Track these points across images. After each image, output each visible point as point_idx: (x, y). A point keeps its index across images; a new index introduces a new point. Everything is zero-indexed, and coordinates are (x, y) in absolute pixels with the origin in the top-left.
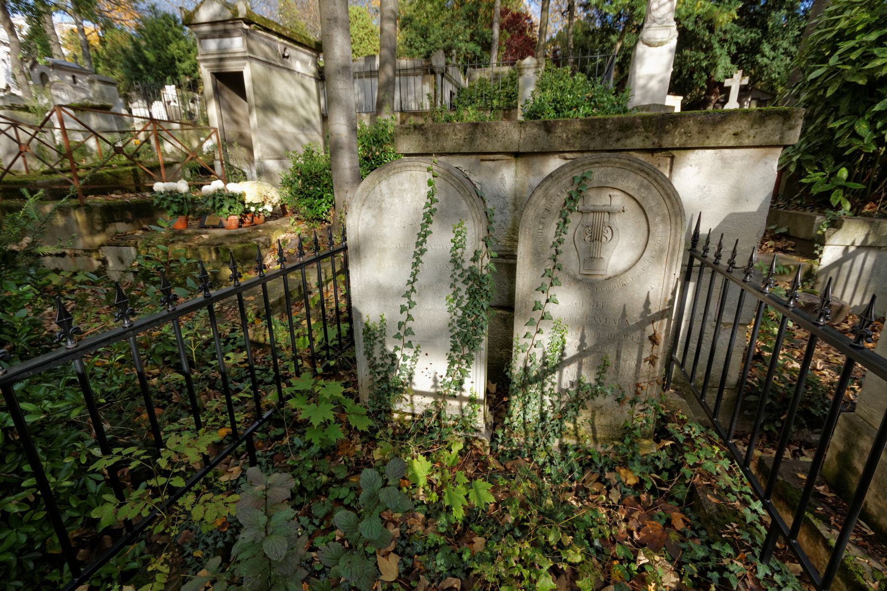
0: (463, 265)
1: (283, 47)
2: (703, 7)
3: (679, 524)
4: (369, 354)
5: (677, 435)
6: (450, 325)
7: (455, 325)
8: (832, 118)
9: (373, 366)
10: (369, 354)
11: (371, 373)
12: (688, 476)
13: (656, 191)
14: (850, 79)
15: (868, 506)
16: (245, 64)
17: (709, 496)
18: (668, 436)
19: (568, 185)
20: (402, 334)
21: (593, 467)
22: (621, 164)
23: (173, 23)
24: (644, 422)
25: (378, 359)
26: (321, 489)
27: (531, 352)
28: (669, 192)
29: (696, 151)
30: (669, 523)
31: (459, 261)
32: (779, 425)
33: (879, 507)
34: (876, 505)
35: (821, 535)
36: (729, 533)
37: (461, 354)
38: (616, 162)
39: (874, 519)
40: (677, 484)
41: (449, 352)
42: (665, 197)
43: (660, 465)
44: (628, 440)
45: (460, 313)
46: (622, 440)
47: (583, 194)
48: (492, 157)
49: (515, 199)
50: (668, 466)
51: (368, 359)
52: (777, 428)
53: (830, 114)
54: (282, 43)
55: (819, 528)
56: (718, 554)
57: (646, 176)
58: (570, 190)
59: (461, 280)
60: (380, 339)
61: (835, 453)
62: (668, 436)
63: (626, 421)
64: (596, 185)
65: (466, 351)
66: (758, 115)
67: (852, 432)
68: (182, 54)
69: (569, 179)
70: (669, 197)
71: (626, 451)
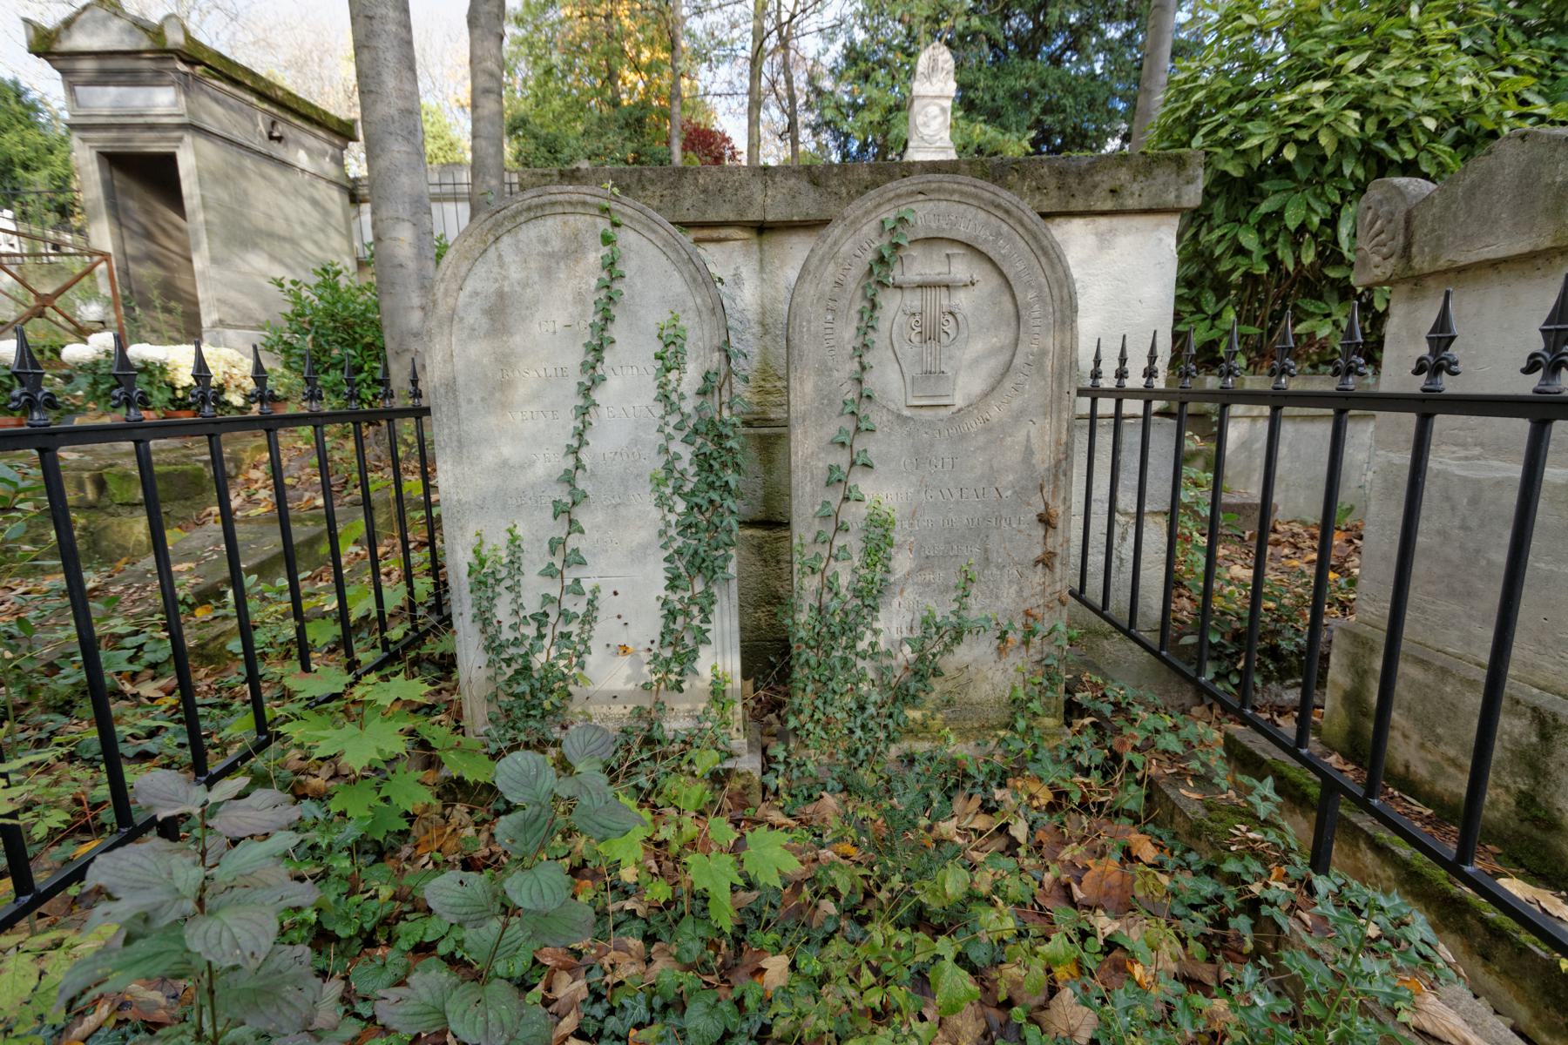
0: (683, 404)
1: (269, 120)
2: (985, 133)
3: (1148, 852)
4: (484, 619)
5: (1098, 705)
6: (662, 533)
7: (673, 532)
8: (1204, 230)
9: (493, 647)
10: (484, 619)
11: (490, 664)
12: (1138, 765)
13: (1022, 244)
14: (1222, 167)
15: (1412, 768)
16: (180, 139)
17: (1183, 791)
18: (1082, 711)
19: (873, 235)
20: (559, 566)
21: (968, 785)
22: (962, 193)
23: (12, 95)
24: (1046, 683)
25: (505, 627)
26: (374, 931)
27: (828, 573)
28: (1045, 243)
29: (1058, 220)
30: (1128, 856)
31: (674, 397)
32: (1236, 680)
33: (1431, 763)
34: (1424, 761)
35: (1361, 830)
36: (1240, 843)
37: (688, 595)
38: (953, 192)
39: (1427, 788)
40: (1124, 786)
41: (663, 594)
42: (1039, 253)
43: (1083, 759)
44: (1021, 724)
45: (681, 506)
46: (1011, 727)
47: (902, 253)
48: (715, 233)
49: (763, 314)
50: (1098, 759)
51: (483, 631)
52: (1234, 686)
53: (1201, 225)
54: (265, 111)
55: (1354, 820)
56: (1234, 879)
57: (1005, 216)
58: (877, 244)
59: (679, 436)
60: (508, 583)
61: (1339, 695)
62: (1082, 711)
63: (1014, 688)
64: (922, 235)
65: (699, 587)
66: (1141, 160)
67: (1360, 651)
68: (32, 154)
69: (875, 223)
70: (1045, 253)
71: (1021, 745)
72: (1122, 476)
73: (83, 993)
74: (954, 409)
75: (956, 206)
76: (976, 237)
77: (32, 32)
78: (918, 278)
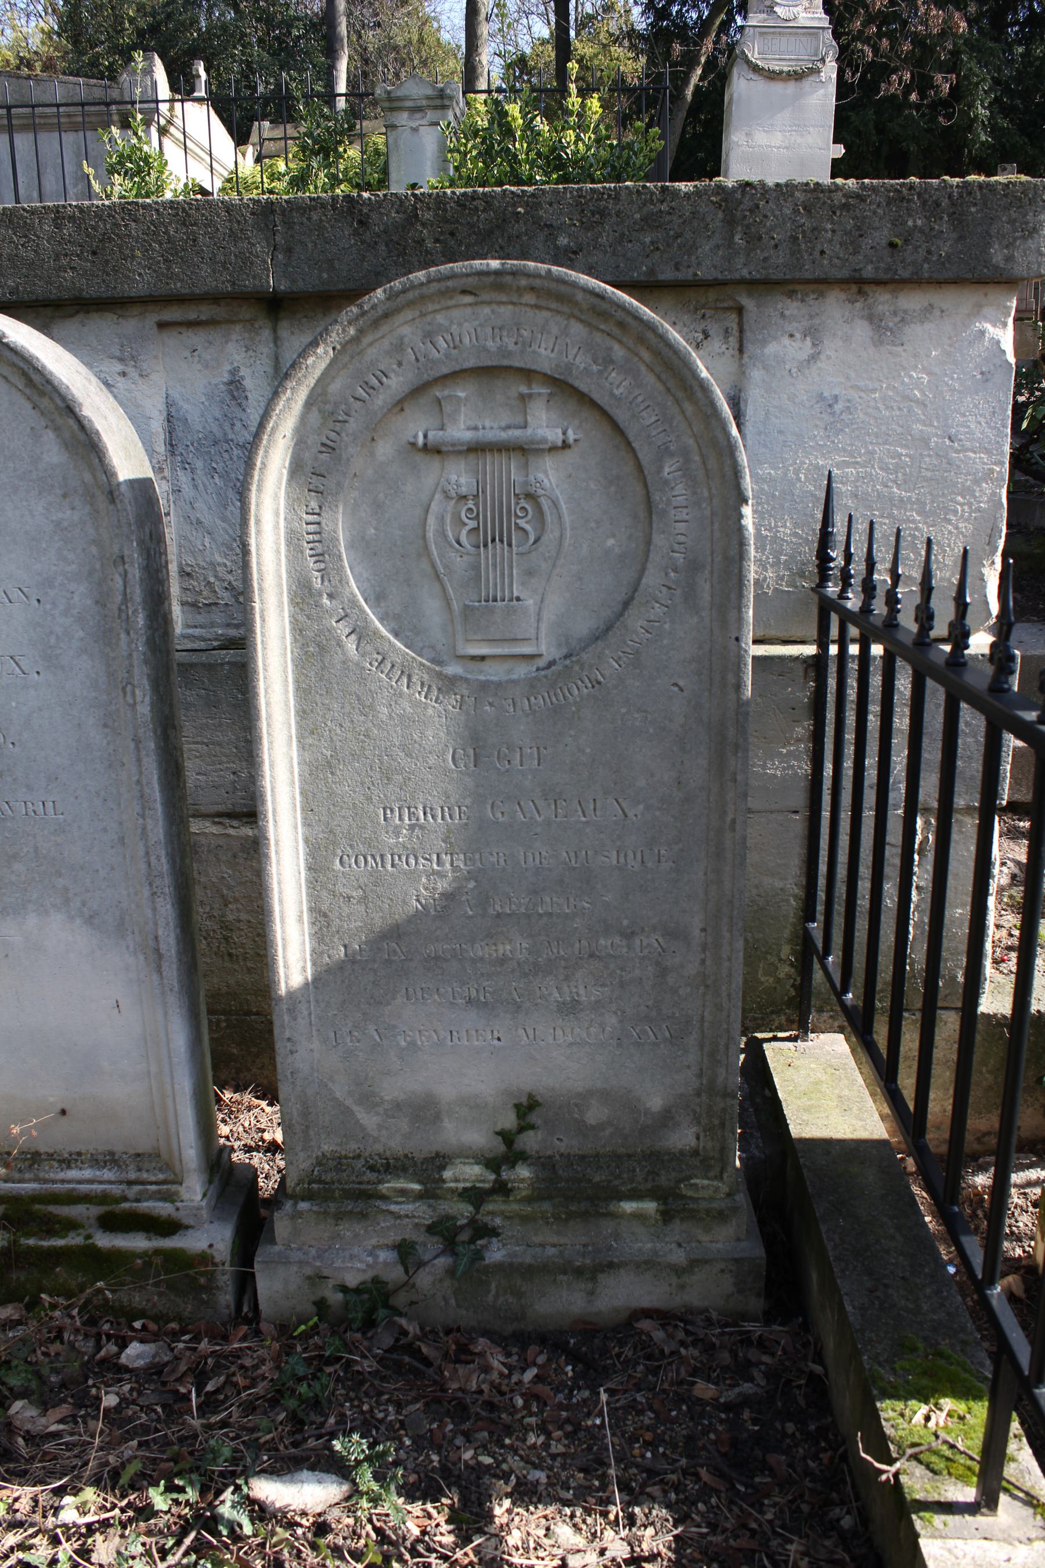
57: (616, 331)
72: (926, 741)
73: (67, 1162)
74: (542, 663)
75: (530, 313)
76: (569, 367)
77: (390, 1287)
78: (468, 436)
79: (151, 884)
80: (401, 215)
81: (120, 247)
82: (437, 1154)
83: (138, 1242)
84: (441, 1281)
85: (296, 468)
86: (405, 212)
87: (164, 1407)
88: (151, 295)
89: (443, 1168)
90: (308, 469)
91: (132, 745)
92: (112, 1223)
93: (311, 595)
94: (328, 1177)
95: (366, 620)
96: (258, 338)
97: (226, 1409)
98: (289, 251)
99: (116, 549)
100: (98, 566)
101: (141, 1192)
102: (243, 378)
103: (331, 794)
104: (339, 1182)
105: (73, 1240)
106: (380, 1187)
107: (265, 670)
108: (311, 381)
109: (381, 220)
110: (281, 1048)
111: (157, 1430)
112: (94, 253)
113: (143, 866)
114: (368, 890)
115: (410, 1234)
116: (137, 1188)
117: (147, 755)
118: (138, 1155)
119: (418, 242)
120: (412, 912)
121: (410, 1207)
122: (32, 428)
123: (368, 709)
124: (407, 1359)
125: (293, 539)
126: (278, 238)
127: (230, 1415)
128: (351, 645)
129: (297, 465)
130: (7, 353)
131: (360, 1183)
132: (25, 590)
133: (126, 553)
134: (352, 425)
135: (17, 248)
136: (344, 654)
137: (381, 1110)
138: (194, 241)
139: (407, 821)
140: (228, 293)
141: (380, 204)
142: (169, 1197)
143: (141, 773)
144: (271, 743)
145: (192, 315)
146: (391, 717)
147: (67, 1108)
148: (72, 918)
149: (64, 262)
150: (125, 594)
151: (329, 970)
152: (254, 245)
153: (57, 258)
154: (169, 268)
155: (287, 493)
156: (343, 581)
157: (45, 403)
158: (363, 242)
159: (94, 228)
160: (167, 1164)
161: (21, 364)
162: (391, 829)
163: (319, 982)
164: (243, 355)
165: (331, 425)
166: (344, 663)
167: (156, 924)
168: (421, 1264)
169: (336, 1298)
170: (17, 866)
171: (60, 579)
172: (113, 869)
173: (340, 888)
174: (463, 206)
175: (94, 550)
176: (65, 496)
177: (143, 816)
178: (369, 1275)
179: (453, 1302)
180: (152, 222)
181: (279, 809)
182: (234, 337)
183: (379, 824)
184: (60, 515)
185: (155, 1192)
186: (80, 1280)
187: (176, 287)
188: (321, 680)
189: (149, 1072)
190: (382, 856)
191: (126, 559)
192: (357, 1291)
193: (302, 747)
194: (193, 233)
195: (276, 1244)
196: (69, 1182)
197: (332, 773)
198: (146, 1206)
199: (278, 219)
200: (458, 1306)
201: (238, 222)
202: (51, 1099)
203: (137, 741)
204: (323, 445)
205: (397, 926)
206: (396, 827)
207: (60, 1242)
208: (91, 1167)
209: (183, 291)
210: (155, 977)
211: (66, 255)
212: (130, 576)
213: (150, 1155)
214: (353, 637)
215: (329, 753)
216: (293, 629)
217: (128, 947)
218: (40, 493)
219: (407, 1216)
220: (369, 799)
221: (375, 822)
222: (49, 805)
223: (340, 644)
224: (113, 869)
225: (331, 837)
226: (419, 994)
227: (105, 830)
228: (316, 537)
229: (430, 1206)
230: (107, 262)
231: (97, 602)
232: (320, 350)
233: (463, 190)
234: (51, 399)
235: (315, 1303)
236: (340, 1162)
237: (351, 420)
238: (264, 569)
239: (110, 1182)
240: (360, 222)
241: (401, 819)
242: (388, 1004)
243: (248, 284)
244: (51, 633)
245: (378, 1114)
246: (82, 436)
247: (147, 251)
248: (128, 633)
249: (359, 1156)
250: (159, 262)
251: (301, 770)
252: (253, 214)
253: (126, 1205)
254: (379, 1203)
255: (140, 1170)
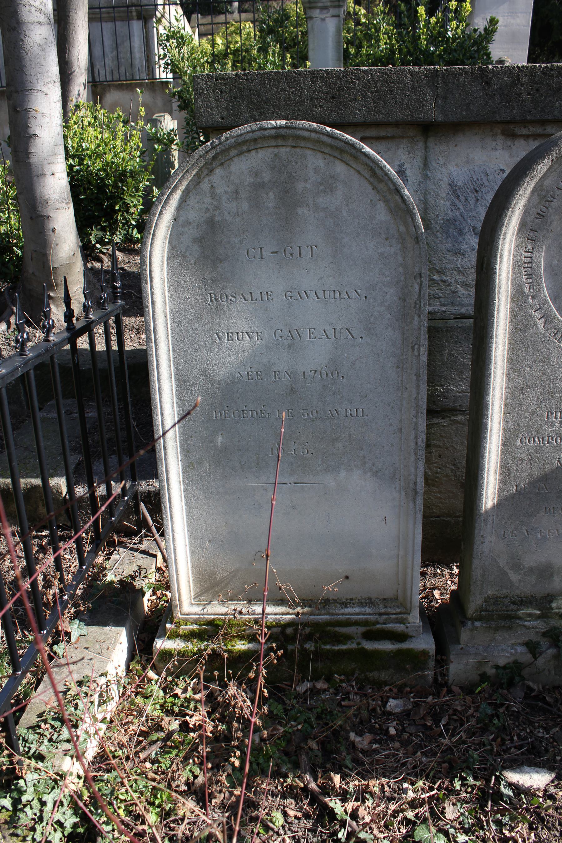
73: (345, 604)
79: (416, 454)
80: (510, 79)
81: (349, 95)
82: (548, 595)
83: (387, 646)
84: (549, 661)
85: (522, 226)
86: (512, 77)
87: (423, 733)
88: (365, 122)
89: (551, 601)
90: (529, 227)
91: (415, 378)
92: (370, 636)
93: (523, 296)
94: (491, 608)
95: (551, 311)
96: (416, 147)
97: (458, 734)
98: (445, 98)
99: (417, 269)
100: (402, 279)
101: (386, 619)
102: (406, 169)
103: (521, 404)
104: (497, 611)
105: (353, 646)
106: (518, 613)
107: (497, 338)
108: (537, 179)
109: (498, 81)
110: (477, 540)
111: (426, 746)
112: (333, 98)
113: (412, 444)
114: (533, 456)
115: (535, 638)
116: (385, 617)
117: (423, 384)
118: (385, 599)
119: (518, 95)
120: (554, 466)
121: (535, 623)
122: (371, 201)
123: (546, 359)
124: (540, 704)
125: (516, 266)
126: (439, 91)
127: (461, 737)
128: (541, 324)
129: (523, 225)
130: (363, 158)
131: (507, 611)
132: (359, 291)
133: (423, 271)
134: (555, 204)
135: (289, 94)
136: (537, 329)
137: (522, 572)
138: (392, 92)
139: (559, 419)
140: (409, 121)
141: (498, 72)
142: (402, 621)
143: (418, 393)
144: (495, 377)
145: (383, 134)
146: (557, 363)
147: (348, 575)
148: (365, 473)
149: (316, 102)
150: (420, 295)
151: (506, 499)
152: (425, 95)
153: (312, 100)
154: (376, 107)
155: (516, 240)
156: (541, 290)
157: (381, 186)
158: (487, 94)
159: (334, 83)
160: (401, 604)
161: (371, 164)
162: (550, 423)
163: (498, 506)
164: (407, 156)
165: (543, 203)
166: (536, 334)
167: (416, 476)
168: (541, 653)
169: (491, 672)
170: (337, 445)
171: (379, 285)
172: (393, 445)
173: (518, 455)
174: (545, 74)
175: (401, 269)
176: (387, 239)
177: (416, 417)
178: (511, 659)
179: (553, 672)
180: (368, 81)
181: (494, 413)
182: (402, 146)
183: (544, 420)
184: (383, 250)
185: (394, 619)
186: (353, 666)
187: (380, 117)
188: (523, 343)
189: (398, 555)
190: (543, 438)
191: (423, 275)
192: (504, 668)
193: (508, 379)
194: (391, 87)
195: (460, 644)
196: (346, 614)
197: (523, 393)
198: (390, 626)
199: (440, 80)
200: (555, 674)
201: (417, 81)
202: (340, 571)
203: (418, 376)
204: (538, 214)
205: (546, 475)
206: (553, 422)
207: (344, 647)
208: (358, 606)
209: (383, 120)
210: (411, 504)
211: (317, 98)
212: (424, 284)
213: (391, 599)
214: (543, 320)
215: (522, 383)
216: (511, 315)
217: (395, 488)
218: (373, 237)
219: (533, 628)
220: (540, 407)
221: (542, 420)
222: (360, 411)
223: (535, 324)
224: (393, 445)
225: (518, 428)
226: (552, 511)
227: (391, 424)
228: (529, 265)
229: (545, 622)
230: (341, 102)
231: (400, 299)
232: (545, 161)
233: (545, 65)
234: (387, 184)
235: (480, 675)
236: (496, 600)
237: (555, 200)
238: (502, 282)
239: (370, 614)
240: (487, 83)
241: (556, 418)
242: (535, 516)
243: (421, 116)
244: (372, 315)
245: (520, 574)
246: (402, 206)
247: (364, 97)
248: (419, 316)
249: (507, 597)
250: (370, 103)
251: (506, 392)
252: (426, 77)
253: (378, 626)
254: (518, 621)
255: (386, 607)
